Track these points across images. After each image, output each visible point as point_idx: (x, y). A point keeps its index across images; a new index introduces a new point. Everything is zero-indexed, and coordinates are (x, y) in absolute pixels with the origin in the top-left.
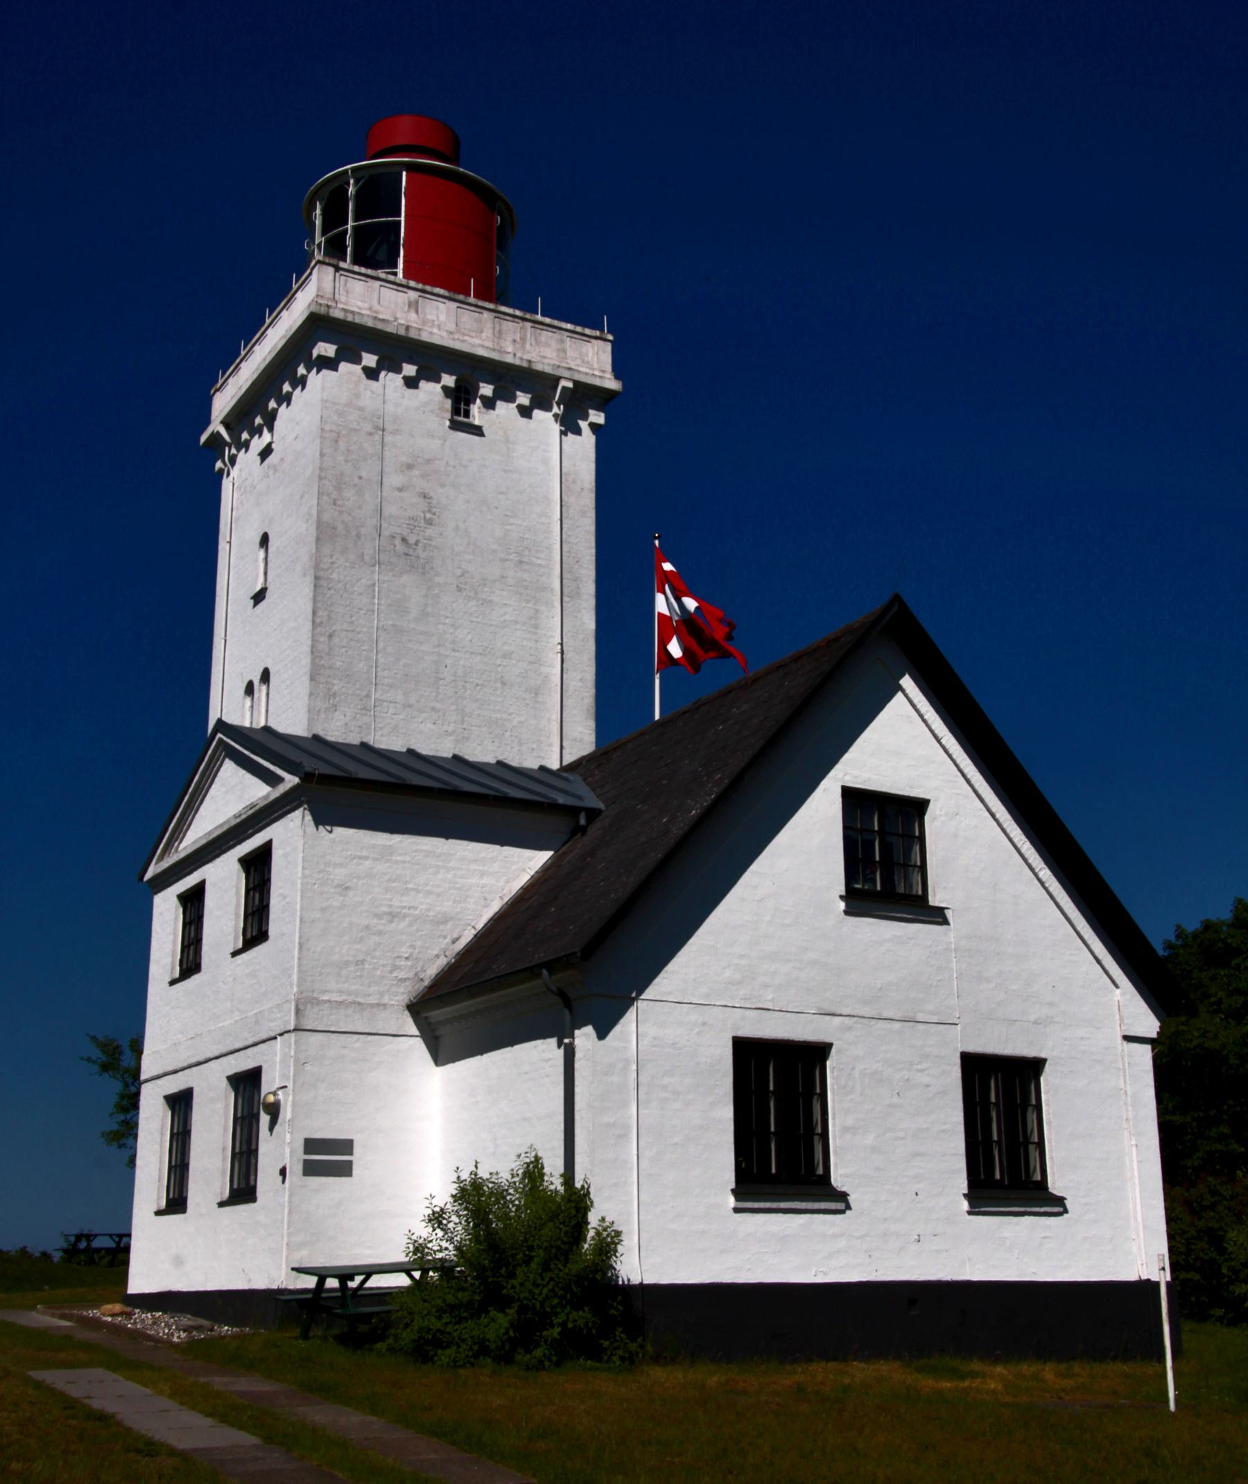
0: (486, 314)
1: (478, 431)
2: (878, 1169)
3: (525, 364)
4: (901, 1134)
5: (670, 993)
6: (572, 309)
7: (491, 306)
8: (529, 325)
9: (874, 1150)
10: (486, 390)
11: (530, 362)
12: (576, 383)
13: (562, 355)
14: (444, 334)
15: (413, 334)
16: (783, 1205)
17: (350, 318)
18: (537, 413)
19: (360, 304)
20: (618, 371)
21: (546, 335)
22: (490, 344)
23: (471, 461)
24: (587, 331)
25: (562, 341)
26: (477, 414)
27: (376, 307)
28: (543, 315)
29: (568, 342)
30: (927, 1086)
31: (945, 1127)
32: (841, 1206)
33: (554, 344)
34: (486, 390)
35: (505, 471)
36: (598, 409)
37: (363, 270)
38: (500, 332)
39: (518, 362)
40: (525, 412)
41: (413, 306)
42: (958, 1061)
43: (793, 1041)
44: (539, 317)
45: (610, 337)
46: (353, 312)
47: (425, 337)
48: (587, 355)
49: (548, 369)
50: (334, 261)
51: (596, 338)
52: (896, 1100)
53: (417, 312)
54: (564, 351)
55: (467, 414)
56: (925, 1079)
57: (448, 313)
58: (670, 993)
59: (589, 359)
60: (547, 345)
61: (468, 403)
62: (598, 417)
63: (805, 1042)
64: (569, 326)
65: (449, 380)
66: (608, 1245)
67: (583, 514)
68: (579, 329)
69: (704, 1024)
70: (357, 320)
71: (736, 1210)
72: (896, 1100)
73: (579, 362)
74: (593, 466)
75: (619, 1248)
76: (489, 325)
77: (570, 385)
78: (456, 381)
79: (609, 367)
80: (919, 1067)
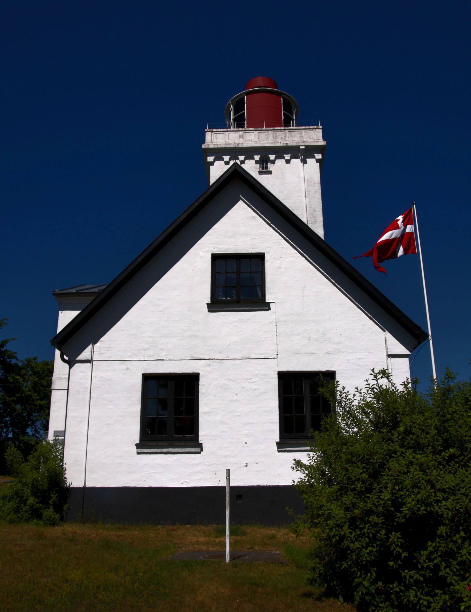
0: (270, 132)
1: (270, 173)
2: (222, 431)
3: (285, 145)
4: (239, 414)
5: (110, 357)
6: (306, 121)
7: (272, 129)
8: (287, 131)
9: (222, 423)
10: (272, 157)
11: (287, 143)
12: (306, 146)
13: (301, 138)
14: (253, 143)
15: (240, 146)
16: (165, 450)
17: (216, 147)
18: (293, 161)
19: (221, 141)
20: (324, 138)
21: (295, 133)
22: (272, 142)
23: (268, 184)
24: (311, 127)
25: (301, 133)
26: (271, 167)
27: (227, 140)
28: (266, 127)
29: (304, 133)
30: (256, 390)
31: (266, 409)
32: (198, 450)
33: (298, 135)
34: (272, 157)
35: (282, 184)
36: (318, 153)
37: (222, 130)
38: (276, 136)
39: (282, 145)
40: (288, 162)
41: (241, 137)
42: (276, 376)
43: (176, 373)
44: (247, 129)
45: (321, 127)
46: (217, 144)
47: (245, 145)
48: (312, 135)
49: (294, 144)
50: (211, 130)
51: (315, 129)
52: (235, 398)
53: (243, 138)
54: (302, 136)
55: (267, 168)
56: (254, 387)
57: (255, 135)
58: (110, 357)
59: (314, 136)
60: (294, 136)
61: (267, 164)
62: (319, 156)
63: (183, 373)
64: (304, 127)
65: (257, 158)
66: (65, 474)
67: (316, 192)
68: (308, 127)
69: (127, 369)
70: (219, 147)
71: (138, 453)
72: (235, 398)
73: (308, 139)
74: (319, 174)
75: (66, 472)
76: (271, 135)
77: (304, 147)
78: (260, 158)
79: (321, 138)
80: (250, 381)
